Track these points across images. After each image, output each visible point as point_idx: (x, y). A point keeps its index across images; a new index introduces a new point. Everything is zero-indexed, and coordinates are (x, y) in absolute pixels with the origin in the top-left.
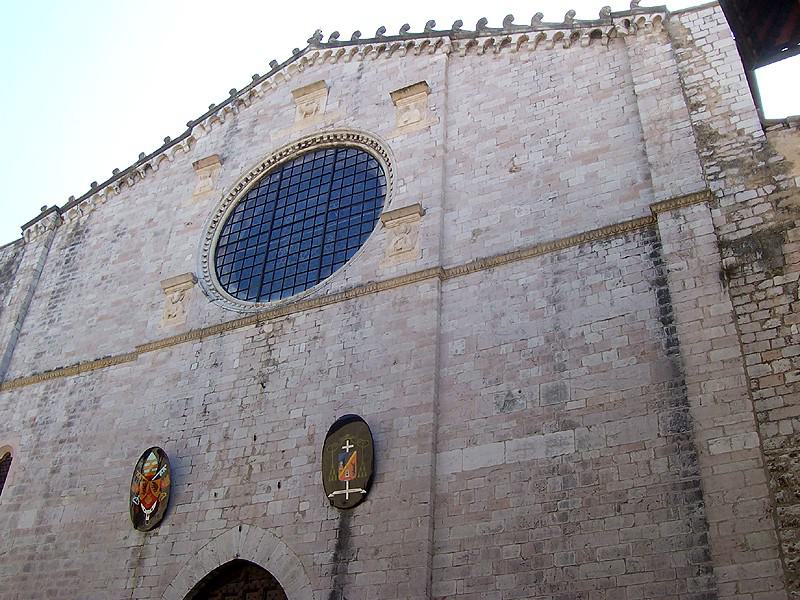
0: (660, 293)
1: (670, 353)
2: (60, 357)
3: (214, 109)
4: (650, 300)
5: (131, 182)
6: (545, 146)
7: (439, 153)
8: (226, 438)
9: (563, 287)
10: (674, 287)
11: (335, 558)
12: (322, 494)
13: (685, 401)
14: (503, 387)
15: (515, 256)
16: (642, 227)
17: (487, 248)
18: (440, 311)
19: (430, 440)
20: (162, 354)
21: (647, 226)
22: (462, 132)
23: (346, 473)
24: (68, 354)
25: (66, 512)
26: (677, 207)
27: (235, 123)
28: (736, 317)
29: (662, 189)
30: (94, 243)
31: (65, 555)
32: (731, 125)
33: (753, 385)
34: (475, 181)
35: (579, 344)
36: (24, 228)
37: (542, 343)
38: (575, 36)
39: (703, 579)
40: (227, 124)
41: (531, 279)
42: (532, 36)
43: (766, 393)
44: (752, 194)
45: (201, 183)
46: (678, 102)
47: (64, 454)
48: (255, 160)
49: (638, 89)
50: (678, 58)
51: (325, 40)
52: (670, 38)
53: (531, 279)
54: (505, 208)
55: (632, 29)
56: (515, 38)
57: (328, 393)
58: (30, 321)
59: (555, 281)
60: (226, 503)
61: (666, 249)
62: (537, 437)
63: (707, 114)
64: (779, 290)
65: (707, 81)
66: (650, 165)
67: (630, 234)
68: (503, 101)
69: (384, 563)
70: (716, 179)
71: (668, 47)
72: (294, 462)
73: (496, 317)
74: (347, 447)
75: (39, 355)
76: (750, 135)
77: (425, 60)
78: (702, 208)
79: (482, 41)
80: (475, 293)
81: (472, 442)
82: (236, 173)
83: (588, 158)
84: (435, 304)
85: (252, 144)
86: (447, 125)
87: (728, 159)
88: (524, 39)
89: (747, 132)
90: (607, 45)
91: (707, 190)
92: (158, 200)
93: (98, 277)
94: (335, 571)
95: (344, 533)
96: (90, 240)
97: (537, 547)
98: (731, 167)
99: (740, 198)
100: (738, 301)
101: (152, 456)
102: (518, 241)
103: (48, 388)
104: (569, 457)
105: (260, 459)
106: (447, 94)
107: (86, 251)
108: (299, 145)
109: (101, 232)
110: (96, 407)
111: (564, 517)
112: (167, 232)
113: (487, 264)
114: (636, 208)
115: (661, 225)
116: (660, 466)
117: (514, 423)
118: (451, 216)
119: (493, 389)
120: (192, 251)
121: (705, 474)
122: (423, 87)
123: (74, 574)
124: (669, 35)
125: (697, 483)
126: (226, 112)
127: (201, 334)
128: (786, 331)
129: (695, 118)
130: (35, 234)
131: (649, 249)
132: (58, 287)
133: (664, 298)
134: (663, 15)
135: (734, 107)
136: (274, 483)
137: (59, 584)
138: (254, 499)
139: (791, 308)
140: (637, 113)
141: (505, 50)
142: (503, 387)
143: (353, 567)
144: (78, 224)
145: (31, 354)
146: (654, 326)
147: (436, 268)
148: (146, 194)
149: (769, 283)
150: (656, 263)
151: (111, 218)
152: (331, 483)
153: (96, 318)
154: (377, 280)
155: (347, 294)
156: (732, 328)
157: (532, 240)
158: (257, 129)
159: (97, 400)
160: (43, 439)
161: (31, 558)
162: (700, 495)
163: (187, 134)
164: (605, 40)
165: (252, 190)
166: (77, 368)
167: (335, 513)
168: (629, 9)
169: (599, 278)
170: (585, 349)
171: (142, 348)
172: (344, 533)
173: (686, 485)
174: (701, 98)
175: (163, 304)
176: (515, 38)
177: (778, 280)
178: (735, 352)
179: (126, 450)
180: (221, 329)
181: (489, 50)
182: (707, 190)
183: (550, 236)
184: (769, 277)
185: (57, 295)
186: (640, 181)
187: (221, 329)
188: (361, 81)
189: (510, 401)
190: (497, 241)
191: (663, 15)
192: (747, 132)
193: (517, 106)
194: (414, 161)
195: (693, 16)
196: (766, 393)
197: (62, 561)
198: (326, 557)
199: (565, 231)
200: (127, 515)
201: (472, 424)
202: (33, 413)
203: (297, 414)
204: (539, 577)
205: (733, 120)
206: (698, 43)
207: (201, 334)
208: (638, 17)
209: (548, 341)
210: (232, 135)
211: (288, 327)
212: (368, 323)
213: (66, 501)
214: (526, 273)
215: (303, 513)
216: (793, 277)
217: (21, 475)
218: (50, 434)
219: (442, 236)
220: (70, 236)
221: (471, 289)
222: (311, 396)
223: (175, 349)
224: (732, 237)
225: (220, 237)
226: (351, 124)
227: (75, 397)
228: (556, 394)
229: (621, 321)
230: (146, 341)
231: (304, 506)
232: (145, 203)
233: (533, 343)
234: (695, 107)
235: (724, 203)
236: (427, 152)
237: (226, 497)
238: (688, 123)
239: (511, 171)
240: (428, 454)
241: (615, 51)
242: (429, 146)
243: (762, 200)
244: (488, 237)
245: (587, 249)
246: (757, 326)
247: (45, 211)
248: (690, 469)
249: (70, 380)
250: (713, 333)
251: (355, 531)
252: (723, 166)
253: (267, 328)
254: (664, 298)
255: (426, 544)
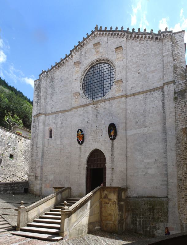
0: (163, 102)
1: (163, 114)
2: (56, 109)
3: (76, 47)
4: (161, 104)
5: (60, 66)
6: (145, 68)
7: (125, 67)
8: (92, 126)
9: (147, 101)
10: (166, 101)
11: (112, 149)
12: (109, 137)
13: (165, 123)
14: (136, 120)
15: (139, 93)
16: (161, 88)
17: (134, 91)
18: (126, 104)
19: (125, 129)
20: (76, 110)
21: (162, 88)
22: (130, 62)
23: (112, 134)
24: (58, 109)
25: (65, 141)
26: (168, 84)
27: (81, 53)
28: (175, 107)
29: (166, 80)
30: (57, 82)
31: (67, 149)
32: (180, 65)
33: (176, 120)
34: (132, 75)
35: (149, 112)
36: (40, 75)
37: (142, 112)
38: (152, 38)
39: (165, 154)
40: (79, 52)
41: (141, 98)
42: (144, 36)
43: (178, 121)
44: (182, 82)
45: (76, 69)
46: (171, 59)
47: (62, 130)
48: (87, 64)
49: (164, 54)
50: (173, 46)
51: (99, 29)
52: (172, 41)
53: (141, 98)
54: (137, 82)
55: (165, 37)
56: (140, 36)
57: (108, 118)
58: (48, 100)
59: (145, 99)
60: (93, 138)
61: (165, 93)
62: (141, 129)
63: (176, 62)
64: (183, 102)
65: (178, 53)
66: (164, 74)
67: (159, 90)
68: (137, 54)
69: (119, 150)
70: (176, 78)
71: (171, 43)
72: (103, 131)
73: (135, 106)
74: (112, 129)
75: (52, 108)
76: (183, 68)
77: (121, 40)
78: (172, 84)
79: (133, 36)
80: (132, 101)
81: (131, 130)
82: (84, 67)
83: (153, 72)
84: (125, 103)
85: (86, 59)
86: (126, 60)
87: (179, 73)
88: (142, 37)
89: (183, 67)
90: (159, 42)
91: (174, 81)
92: (68, 72)
93: (60, 91)
94: (112, 151)
95: (113, 144)
96: (56, 81)
97: (142, 148)
98: (179, 75)
99: (180, 82)
100: (176, 104)
101: (79, 131)
102: (139, 90)
103: (55, 116)
104: (146, 132)
105: (99, 130)
106: (126, 51)
107: (55, 84)
108: (96, 61)
109: (58, 79)
110: (66, 120)
111: (146, 143)
112: (71, 81)
113: (134, 95)
114: (160, 84)
115: (165, 88)
116: (161, 135)
117: (137, 126)
118: (128, 83)
119: (135, 120)
120: (77, 86)
121: (167, 137)
122: (121, 47)
123: (69, 152)
124: (172, 40)
125: (166, 139)
126: (79, 49)
127: (83, 106)
128: (183, 110)
129: (174, 63)
130: (42, 78)
131: (162, 93)
132: (52, 92)
133: (163, 103)
134: (171, 34)
135: (182, 61)
136: (101, 135)
137: (67, 154)
138: (98, 138)
139: (184, 106)
140: (163, 61)
141: (138, 39)
142: (136, 120)
143: (114, 150)
144: (52, 76)
145: (50, 108)
146: (161, 109)
147: (125, 95)
148: (64, 71)
149: (182, 101)
150: (163, 96)
151: (58, 76)
152: (110, 136)
153: (62, 101)
154: (114, 96)
155: (110, 99)
156: (174, 109)
157: (142, 90)
158: (86, 55)
159: (66, 119)
160: (57, 127)
161: (61, 149)
162: (166, 141)
163: (71, 54)
164: (158, 40)
165: (87, 72)
166: (60, 112)
167: (111, 141)
168: (164, 31)
169: (153, 99)
170: (150, 113)
171: (72, 108)
172: (113, 144)
173: (164, 139)
174: (176, 58)
175: (74, 99)
176: (140, 36)
177: (183, 100)
178: (174, 114)
179: (74, 130)
180: (87, 105)
181: (135, 39)
182: (174, 81)
183: (145, 90)
184: (182, 100)
185: (52, 94)
186: (162, 78)
187: (87, 105)
188: (108, 44)
189: (137, 122)
190: (136, 90)
191: (171, 34)
192: (183, 67)
193: (140, 56)
194: (120, 68)
195: (177, 35)
196: (178, 121)
197: (67, 150)
198: (110, 148)
199: (148, 89)
200: (77, 142)
201: (132, 126)
202: (54, 121)
203: (103, 122)
204: (142, 152)
205: (181, 64)
206: (177, 43)
207: (83, 106)
208: (166, 34)
209: (144, 111)
210: (81, 56)
211: (99, 105)
212: (114, 106)
213: (65, 139)
214: (141, 97)
215: (106, 141)
216: (186, 100)
217: (55, 134)
218: (58, 126)
219: (126, 88)
220: (51, 79)
221: (131, 100)
222: (105, 119)
223: (78, 109)
224: (177, 91)
225: (83, 84)
226: (107, 56)
227: (62, 118)
228: (144, 121)
229: (156, 108)
230: (72, 107)
231: (106, 139)
232: (65, 73)
233: (141, 112)
234: (174, 60)
235: (176, 84)
236: (123, 66)
237: (93, 137)
238: (172, 64)
239: (139, 73)
240: (125, 131)
241: (160, 44)
242: (123, 65)
243: (183, 83)
244: (134, 89)
245: (151, 93)
246: (179, 102)
247: (43, 72)
248: (165, 136)
249: (60, 114)
250: (170, 110)
251: (114, 144)
252: (178, 75)
253: (95, 106)
254: (163, 103)
255: (125, 147)
